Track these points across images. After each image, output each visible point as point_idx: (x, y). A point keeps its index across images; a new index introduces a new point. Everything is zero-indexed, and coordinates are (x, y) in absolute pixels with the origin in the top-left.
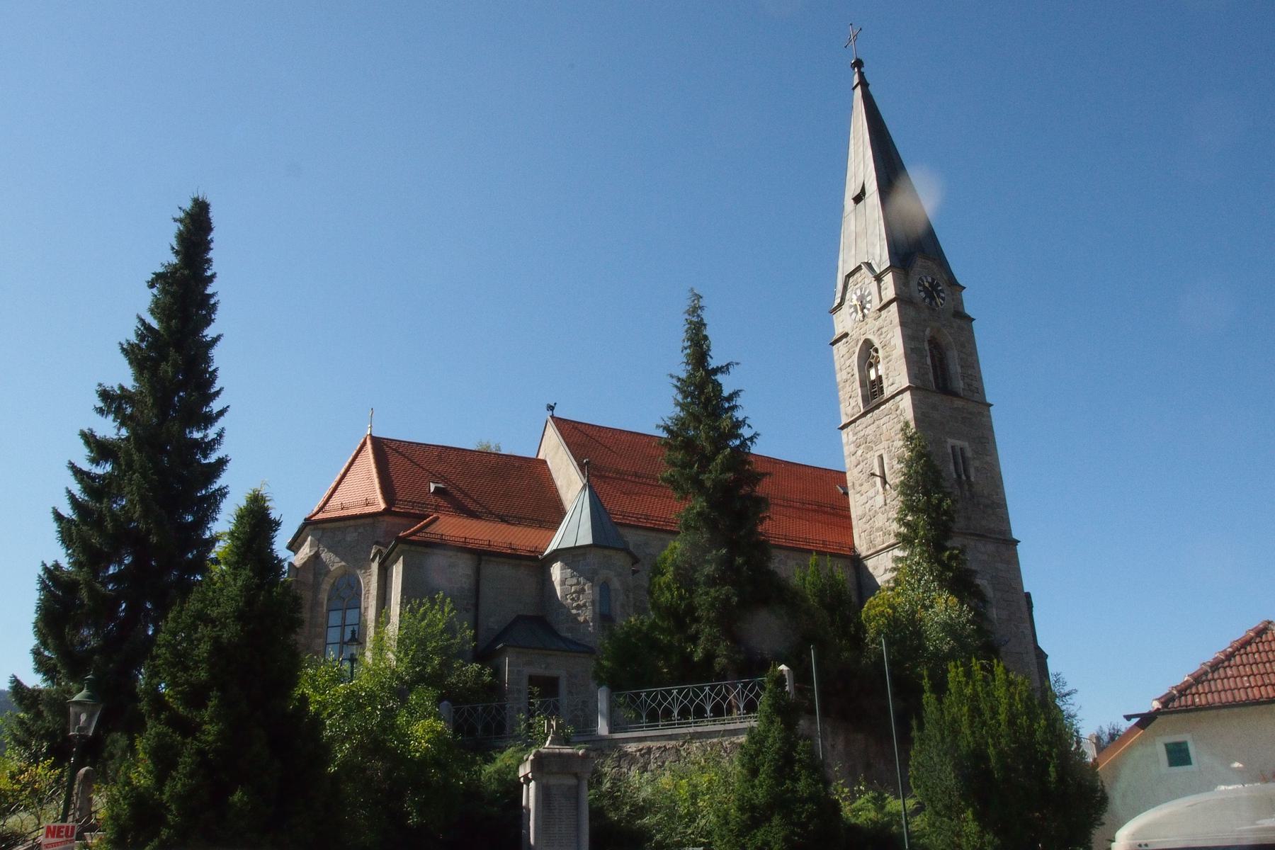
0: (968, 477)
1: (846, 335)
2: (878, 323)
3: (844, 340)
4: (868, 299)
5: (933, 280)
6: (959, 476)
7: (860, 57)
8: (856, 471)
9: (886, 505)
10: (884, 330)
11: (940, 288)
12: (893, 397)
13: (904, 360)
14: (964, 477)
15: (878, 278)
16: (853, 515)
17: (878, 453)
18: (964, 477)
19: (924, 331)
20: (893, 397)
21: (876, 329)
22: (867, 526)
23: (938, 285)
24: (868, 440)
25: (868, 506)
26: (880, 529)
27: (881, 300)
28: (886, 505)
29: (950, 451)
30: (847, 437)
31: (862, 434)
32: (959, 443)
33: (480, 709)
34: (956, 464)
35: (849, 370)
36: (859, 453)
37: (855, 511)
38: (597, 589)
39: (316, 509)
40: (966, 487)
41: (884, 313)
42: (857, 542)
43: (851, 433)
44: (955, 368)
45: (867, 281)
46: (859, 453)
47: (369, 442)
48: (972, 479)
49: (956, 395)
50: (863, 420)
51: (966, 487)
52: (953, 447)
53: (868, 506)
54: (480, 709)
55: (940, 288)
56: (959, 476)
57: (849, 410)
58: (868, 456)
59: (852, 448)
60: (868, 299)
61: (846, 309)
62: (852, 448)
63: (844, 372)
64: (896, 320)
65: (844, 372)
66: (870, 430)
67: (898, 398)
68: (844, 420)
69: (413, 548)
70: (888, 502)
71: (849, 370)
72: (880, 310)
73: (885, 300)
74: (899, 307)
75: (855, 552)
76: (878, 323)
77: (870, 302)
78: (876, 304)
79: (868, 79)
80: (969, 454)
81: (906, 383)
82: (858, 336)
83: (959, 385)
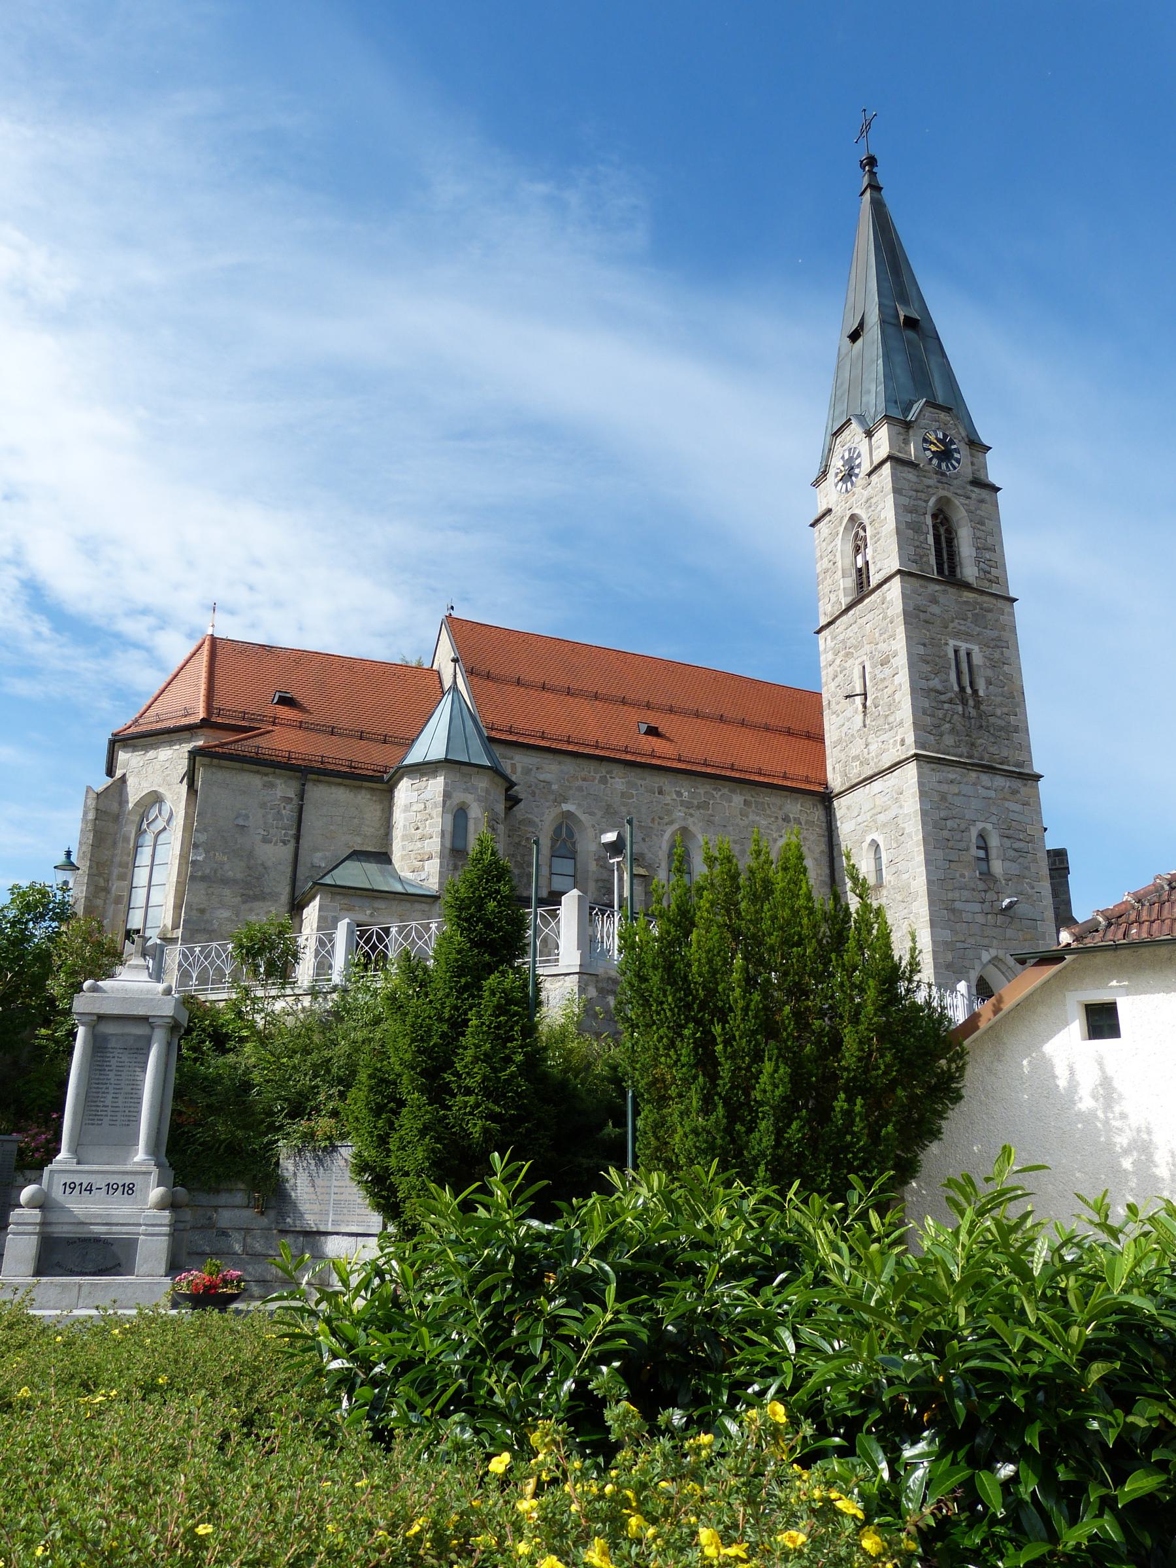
0: (975, 692)
1: (829, 511)
2: (866, 493)
3: (828, 518)
4: (857, 462)
5: (945, 436)
6: (962, 689)
7: (872, 152)
8: (833, 685)
9: (865, 726)
10: (873, 501)
11: (953, 447)
12: (880, 586)
13: (895, 538)
14: (969, 691)
15: (869, 434)
16: (827, 742)
17: (860, 660)
18: (969, 691)
19: (927, 501)
20: (880, 586)
21: (864, 499)
22: (843, 756)
23: (952, 442)
24: (848, 645)
25: (844, 729)
26: (856, 758)
27: (872, 462)
28: (865, 726)
29: (951, 655)
30: (825, 641)
31: (841, 637)
32: (964, 646)
33: (197, 950)
34: (959, 673)
35: (830, 557)
36: (838, 662)
37: (831, 734)
38: (449, 817)
39: (129, 723)
40: (971, 703)
41: (874, 477)
42: (830, 776)
43: (829, 638)
44: (966, 548)
45: (857, 439)
46: (838, 662)
47: (207, 643)
48: (981, 693)
49: (967, 586)
50: (844, 618)
51: (971, 703)
52: (956, 652)
53: (844, 729)
54: (197, 950)
55: (953, 447)
56: (962, 689)
57: (829, 608)
58: (847, 665)
59: (830, 656)
60: (857, 462)
61: (831, 478)
62: (830, 656)
63: (825, 560)
64: (889, 486)
65: (825, 560)
66: (849, 633)
67: (885, 587)
68: (823, 621)
69: (215, 761)
70: (867, 722)
71: (830, 557)
72: (869, 475)
73: (877, 460)
74: (892, 468)
75: (827, 788)
76: (866, 493)
77: (859, 466)
78: (866, 467)
79: (881, 181)
80: (977, 659)
81: (895, 565)
82: (841, 511)
83: (969, 572)
